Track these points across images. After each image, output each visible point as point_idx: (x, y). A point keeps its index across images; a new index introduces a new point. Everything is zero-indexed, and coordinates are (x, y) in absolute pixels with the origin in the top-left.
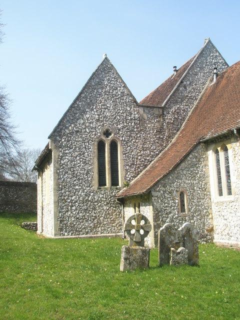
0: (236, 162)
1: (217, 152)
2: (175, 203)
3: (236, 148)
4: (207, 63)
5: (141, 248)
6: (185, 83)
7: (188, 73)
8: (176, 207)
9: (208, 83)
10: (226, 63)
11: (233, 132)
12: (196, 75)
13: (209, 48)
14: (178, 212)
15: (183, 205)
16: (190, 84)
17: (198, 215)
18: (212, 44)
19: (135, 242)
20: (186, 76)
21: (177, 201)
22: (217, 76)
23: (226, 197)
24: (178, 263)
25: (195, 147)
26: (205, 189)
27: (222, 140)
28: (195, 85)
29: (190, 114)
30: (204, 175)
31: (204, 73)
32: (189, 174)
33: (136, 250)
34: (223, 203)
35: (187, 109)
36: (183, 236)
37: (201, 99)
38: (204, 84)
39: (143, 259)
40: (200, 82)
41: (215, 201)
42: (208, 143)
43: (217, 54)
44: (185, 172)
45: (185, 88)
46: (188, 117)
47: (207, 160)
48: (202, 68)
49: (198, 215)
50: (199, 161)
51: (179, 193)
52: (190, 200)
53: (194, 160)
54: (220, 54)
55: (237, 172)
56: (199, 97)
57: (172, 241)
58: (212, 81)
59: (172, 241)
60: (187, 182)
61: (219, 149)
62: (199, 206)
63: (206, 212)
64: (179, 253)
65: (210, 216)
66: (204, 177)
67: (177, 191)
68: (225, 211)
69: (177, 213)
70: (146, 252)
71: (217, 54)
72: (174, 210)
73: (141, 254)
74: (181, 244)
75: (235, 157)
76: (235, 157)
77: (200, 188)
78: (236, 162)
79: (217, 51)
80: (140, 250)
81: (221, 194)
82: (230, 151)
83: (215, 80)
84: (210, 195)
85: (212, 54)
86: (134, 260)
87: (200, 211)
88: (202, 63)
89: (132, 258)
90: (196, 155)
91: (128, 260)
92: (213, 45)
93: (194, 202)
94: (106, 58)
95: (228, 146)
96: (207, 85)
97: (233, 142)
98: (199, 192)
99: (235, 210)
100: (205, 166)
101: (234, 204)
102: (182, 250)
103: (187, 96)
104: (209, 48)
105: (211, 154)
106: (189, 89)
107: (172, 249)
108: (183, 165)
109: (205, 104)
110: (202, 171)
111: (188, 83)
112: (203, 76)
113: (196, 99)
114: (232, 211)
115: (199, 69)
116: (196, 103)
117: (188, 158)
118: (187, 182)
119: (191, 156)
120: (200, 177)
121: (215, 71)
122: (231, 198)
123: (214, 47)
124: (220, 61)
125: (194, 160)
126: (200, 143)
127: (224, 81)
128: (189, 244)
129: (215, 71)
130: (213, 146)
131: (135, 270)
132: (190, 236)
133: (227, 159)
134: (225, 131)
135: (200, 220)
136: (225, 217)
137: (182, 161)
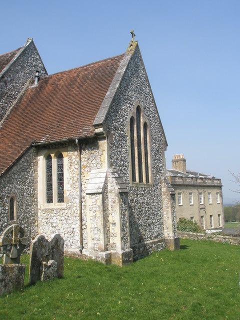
0: (72, 170)
1: (49, 158)
2: (5, 210)
3: (74, 157)
4: (28, 63)
5: (17, 265)
6: (6, 78)
7: (10, 69)
8: (5, 214)
9: (27, 84)
10: (44, 68)
11: (75, 140)
12: (18, 73)
13: (30, 50)
14: (8, 220)
15: (12, 212)
16: (11, 81)
17: (25, 223)
18: (34, 45)
19: (11, 259)
20: (7, 71)
21: (7, 208)
22: (39, 79)
23: (55, 205)
24: (49, 278)
25: (28, 149)
26: (33, 196)
27: (57, 146)
28: (16, 83)
29: (8, 113)
30: (33, 180)
31: (25, 73)
32: (20, 178)
33: (12, 268)
34: (53, 210)
35: (6, 107)
36: (53, 248)
37: (21, 99)
38: (23, 84)
39: (19, 277)
40: (20, 81)
41: (42, 208)
42: (39, 149)
43: (38, 57)
44: (16, 176)
45: (6, 84)
46: (6, 116)
47: (37, 165)
48: (23, 67)
49: (25, 223)
50: (30, 165)
51: (9, 199)
52: (19, 207)
53: (26, 164)
54: (40, 58)
55: (71, 180)
56: (19, 97)
57: (43, 254)
58: (32, 82)
59: (43, 254)
60: (18, 187)
61: (53, 155)
62: (27, 213)
63: (33, 220)
64: (50, 266)
65: (36, 224)
66: (34, 182)
67: (8, 197)
68: (55, 218)
69: (6, 221)
70: (21, 270)
71: (38, 57)
72: (3, 217)
73: (17, 272)
74: (51, 256)
75: (71, 165)
76: (71, 165)
77: (29, 194)
78: (72, 170)
79: (38, 54)
80: (16, 268)
81: (50, 200)
82: (66, 160)
83: (36, 82)
84: (37, 201)
85: (33, 56)
86: (10, 281)
87: (28, 218)
88: (23, 62)
89: (8, 278)
90: (28, 159)
91: (4, 283)
92: (35, 47)
93: (22, 208)
94: (32, 42)
95: (64, 154)
96: (26, 86)
97: (70, 151)
98: (28, 198)
99: (66, 217)
100: (35, 171)
101: (66, 211)
102: (52, 264)
103: (7, 93)
104: (30, 50)
105: (41, 161)
106: (10, 86)
107: (44, 263)
108: (15, 168)
109: (27, 106)
110: (31, 176)
111: (9, 79)
112: (24, 76)
113: (15, 98)
114: (63, 218)
115: (20, 67)
116: (15, 102)
117: (21, 162)
118: (18, 187)
119: (23, 160)
120: (30, 182)
121: (37, 74)
122: (63, 205)
123: (36, 49)
124: (40, 65)
125: (26, 164)
126: (32, 146)
127: (49, 88)
128: (56, 256)
129: (37, 74)
130: (46, 152)
131: (10, 293)
132: (58, 248)
133: (61, 167)
134: (65, 139)
135: (27, 228)
136: (54, 225)
137: (15, 164)
